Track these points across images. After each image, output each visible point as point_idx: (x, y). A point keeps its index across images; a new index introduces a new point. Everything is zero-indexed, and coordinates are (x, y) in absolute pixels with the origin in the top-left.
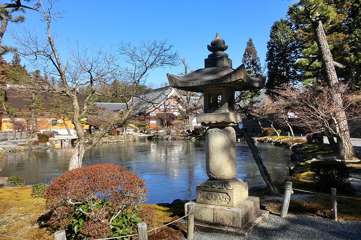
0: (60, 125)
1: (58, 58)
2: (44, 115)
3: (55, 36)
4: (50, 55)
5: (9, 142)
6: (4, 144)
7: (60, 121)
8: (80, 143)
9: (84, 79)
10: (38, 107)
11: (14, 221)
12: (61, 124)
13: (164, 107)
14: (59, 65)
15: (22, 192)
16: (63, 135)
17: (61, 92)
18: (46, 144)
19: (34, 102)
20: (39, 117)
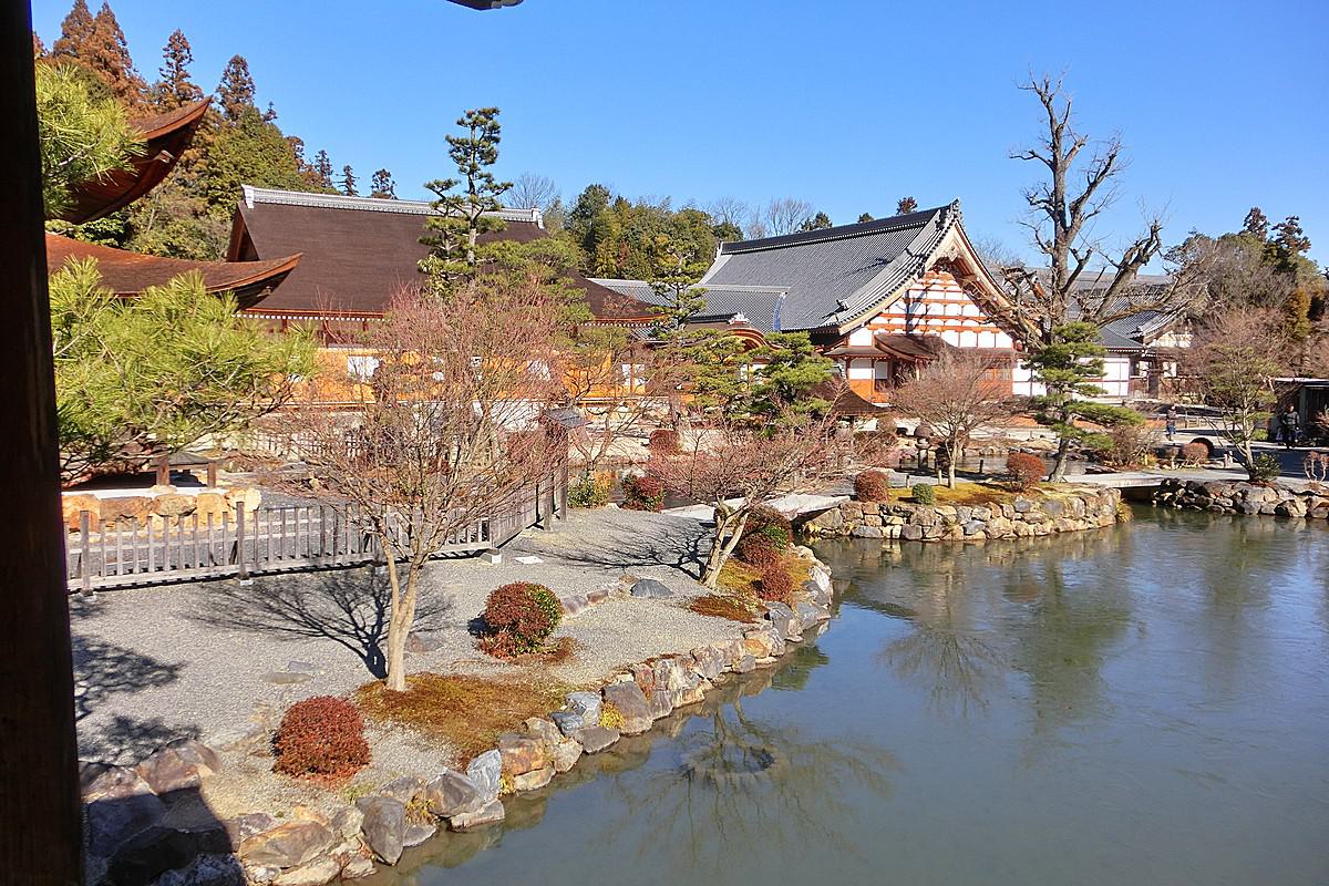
13: (904, 306)
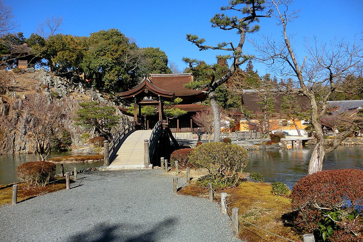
0: (290, 126)
1: (294, 59)
2: (275, 116)
3: (291, 37)
4: (286, 57)
5: (246, 141)
6: (243, 143)
7: (290, 122)
8: (319, 145)
9: (321, 77)
10: (270, 109)
11: (260, 214)
12: (291, 124)
14: (295, 65)
15: (263, 188)
16: (293, 136)
17: (298, 93)
18: (278, 144)
19: (266, 104)
20: (271, 118)
